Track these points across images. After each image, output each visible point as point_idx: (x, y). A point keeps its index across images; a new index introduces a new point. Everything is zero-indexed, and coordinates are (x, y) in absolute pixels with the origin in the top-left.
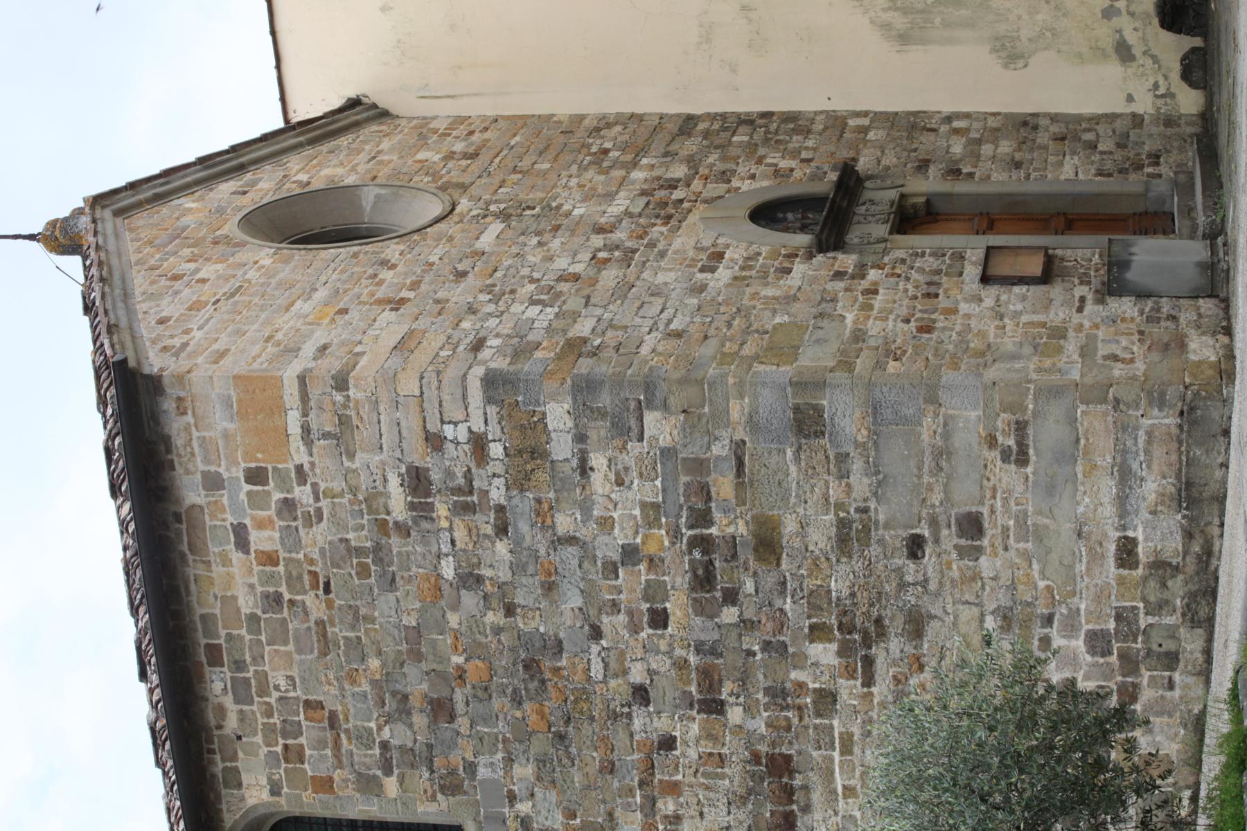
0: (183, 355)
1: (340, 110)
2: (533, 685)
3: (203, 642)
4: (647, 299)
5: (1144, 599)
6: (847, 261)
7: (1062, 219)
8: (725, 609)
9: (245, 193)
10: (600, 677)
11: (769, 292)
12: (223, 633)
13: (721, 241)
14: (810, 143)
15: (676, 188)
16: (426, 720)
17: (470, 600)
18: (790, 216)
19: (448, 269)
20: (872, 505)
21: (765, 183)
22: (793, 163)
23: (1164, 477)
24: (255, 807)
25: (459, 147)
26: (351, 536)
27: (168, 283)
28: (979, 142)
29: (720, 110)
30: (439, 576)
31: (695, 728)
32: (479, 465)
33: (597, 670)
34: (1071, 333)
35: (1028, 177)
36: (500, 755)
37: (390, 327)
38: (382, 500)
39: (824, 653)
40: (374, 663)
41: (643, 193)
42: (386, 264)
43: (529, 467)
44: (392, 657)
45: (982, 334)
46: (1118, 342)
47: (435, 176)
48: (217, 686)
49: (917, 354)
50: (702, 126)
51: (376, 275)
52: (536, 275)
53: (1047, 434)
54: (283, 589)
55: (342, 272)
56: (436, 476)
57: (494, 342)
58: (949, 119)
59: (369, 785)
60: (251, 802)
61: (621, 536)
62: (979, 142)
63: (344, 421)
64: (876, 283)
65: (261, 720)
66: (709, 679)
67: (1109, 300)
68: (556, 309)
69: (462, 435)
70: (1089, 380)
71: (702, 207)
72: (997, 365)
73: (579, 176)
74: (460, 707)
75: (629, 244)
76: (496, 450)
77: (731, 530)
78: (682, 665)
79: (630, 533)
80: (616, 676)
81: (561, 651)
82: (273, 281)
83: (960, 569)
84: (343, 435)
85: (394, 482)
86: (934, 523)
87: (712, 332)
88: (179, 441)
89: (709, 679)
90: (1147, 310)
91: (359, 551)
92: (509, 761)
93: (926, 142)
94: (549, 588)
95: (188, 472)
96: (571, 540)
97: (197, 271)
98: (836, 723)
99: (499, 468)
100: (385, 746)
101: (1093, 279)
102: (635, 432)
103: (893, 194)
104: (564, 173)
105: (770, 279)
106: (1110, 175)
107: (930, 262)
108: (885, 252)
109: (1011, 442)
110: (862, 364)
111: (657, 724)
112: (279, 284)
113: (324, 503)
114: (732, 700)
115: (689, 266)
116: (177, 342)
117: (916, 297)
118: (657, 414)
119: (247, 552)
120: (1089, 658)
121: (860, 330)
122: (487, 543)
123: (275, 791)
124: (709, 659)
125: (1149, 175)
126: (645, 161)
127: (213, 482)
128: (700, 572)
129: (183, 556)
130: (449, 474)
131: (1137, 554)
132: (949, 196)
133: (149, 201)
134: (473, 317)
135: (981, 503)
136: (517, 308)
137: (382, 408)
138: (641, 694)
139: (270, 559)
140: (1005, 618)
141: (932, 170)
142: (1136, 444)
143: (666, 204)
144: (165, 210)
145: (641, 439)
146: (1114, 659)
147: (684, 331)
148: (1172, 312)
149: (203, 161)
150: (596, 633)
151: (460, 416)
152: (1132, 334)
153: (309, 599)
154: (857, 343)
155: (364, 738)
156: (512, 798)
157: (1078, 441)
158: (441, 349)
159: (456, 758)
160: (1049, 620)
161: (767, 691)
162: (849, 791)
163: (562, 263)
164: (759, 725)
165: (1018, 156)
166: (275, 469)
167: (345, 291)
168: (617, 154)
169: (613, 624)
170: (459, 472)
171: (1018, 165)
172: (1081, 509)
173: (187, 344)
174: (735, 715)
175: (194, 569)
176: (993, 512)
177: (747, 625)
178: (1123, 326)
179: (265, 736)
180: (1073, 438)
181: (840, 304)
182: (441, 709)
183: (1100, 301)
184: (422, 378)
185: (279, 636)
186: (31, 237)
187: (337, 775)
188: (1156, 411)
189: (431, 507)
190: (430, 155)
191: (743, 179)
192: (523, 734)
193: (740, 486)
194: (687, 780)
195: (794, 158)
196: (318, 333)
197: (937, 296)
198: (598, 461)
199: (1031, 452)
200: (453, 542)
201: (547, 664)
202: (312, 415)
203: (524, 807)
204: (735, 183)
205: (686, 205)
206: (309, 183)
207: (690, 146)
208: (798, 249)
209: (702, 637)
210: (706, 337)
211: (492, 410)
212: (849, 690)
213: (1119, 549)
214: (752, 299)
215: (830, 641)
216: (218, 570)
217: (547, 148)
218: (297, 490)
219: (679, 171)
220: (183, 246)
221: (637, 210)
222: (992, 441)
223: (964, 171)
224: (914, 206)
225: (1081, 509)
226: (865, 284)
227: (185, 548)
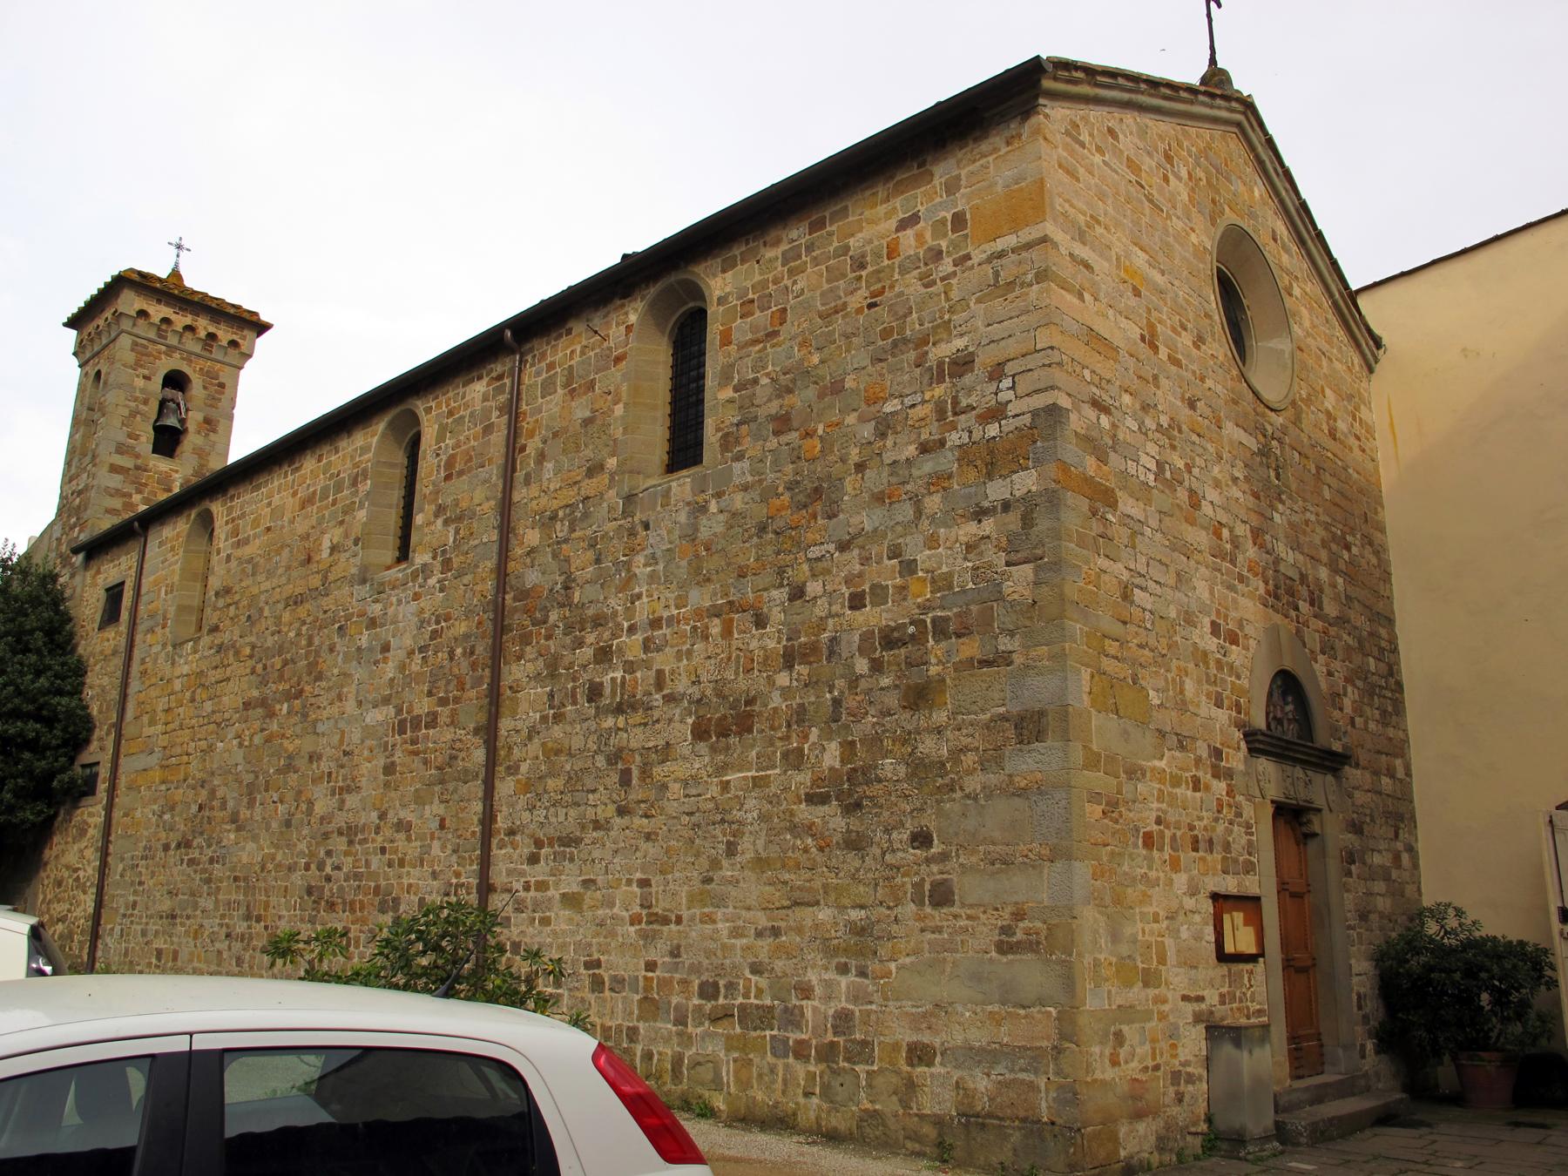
0: (1068, 140)
1: (1369, 331)
2: (801, 497)
3: (827, 214)
4: (1172, 569)
5: (881, 1070)
6: (1236, 759)
7: (1309, 963)
8: (866, 661)
9: (1275, 240)
10: (810, 555)
11: (1189, 686)
12: (834, 228)
13: (1252, 643)
14: (1372, 726)
15: (1312, 604)
16: (773, 412)
17: (867, 431)
18: (1289, 708)
19: (1199, 394)
20: (958, 794)
21: (1324, 686)
22: (1348, 709)
23: (990, 1099)
24: (709, 286)
25: (1342, 426)
26: (914, 315)
27: (1161, 150)
28: (1387, 878)
29: (1401, 648)
30: (885, 400)
31: (771, 644)
32: (978, 416)
33: (815, 552)
34: (1152, 992)
35: (1350, 927)
36: (750, 479)
37: (1123, 332)
38: (945, 336)
39: (832, 756)
40: (816, 359)
41: (1303, 578)
42: (1199, 341)
43: (979, 463)
44: (820, 372)
45: (1145, 899)
46: (1142, 1043)
47: (1308, 401)
48: (794, 234)
49: (1114, 834)
50: (1383, 632)
51: (1185, 329)
52: (1196, 471)
53: (1030, 973)
54: (870, 269)
55: (1187, 301)
56: (968, 379)
57: (1105, 421)
58: (1411, 849)
59: (726, 377)
60: (712, 283)
61: (923, 557)
62: (1387, 878)
63: (1010, 285)
64: (1208, 788)
65: (771, 276)
66: (808, 654)
67: (1201, 1028)
68: (1152, 484)
69: (1005, 396)
70: (1083, 1020)
71: (1292, 627)
72: (1102, 919)
73: (1318, 522)
74: (784, 439)
75: (1240, 558)
76: (993, 430)
77: (933, 660)
78: (821, 626)
79: (927, 565)
80: (811, 569)
81: (830, 518)
82: (1171, 239)
83: (904, 884)
84: (1000, 288)
85: (959, 343)
86: (944, 857)
87: (1132, 628)
88: (985, 146)
89: (808, 654)
90: (1189, 1069)
91: (902, 329)
92: (745, 488)
93: (1382, 830)
94: (879, 498)
95: (959, 162)
96: (919, 513)
97: (1179, 179)
98: (777, 771)
99: (977, 436)
100: (755, 381)
101: (1228, 1006)
102: (1014, 557)
103: (1319, 802)
104: (1321, 510)
105: (1206, 686)
106: (1360, 1008)
107: (1239, 838)
108: (1250, 798)
109: (1019, 936)
110: (1098, 780)
111: (776, 610)
112: (1168, 244)
113: (940, 285)
114: (795, 675)
115: (1218, 612)
116: (1085, 137)
117: (1191, 828)
118: (1031, 577)
119: (897, 230)
120: (831, 1012)
121: (1144, 775)
122: (914, 436)
123: (722, 301)
124: (825, 652)
125: (1363, 1046)
126: (1340, 580)
127: (952, 187)
128: (896, 634)
129: (892, 178)
130: (970, 391)
131: (919, 1065)
132: (1323, 853)
133: (1257, 157)
134: (1138, 406)
135: (963, 905)
136: (1152, 449)
137: (1023, 318)
138: (798, 593)
139: (892, 252)
140: (863, 929)
141: (1350, 839)
142: (1022, 1070)
143: (1293, 595)
144: (1249, 170)
145: (1008, 564)
146: (830, 1037)
147: (1132, 602)
148: (1187, 1098)
149: (1304, 206)
150: (843, 547)
151: (1020, 390)
152: (1154, 1058)
153: (863, 292)
154: (1126, 772)
155: (759, 365)
156: (719, 495)
157: (1024, 1007)
158: (1093, 372)
159: (747, 443)
160: (862, 973)
161: (802, 706)
162: (725, 786)
163: (1212, 495)
164: (776, 700)
165: (1373, 917)
166: (966, 236)
167: (1164, 300)
168: (1346, 556)
169: (851, 561)
170: (973, 400)
171: (1363, 917)
172: (960, 1009)
173: (1083, 145)
174: (783, 679)
175: (881, 191)
176: (955, 917)
177: (854, 682)
178: (1164, 1045)
179: (759, 282)
180: (1026, 1003)
181: (1177, 754)
182: (782, 423)
183: (1198, 1018)
184: (1052, 348)
185: (834, 275)
186: (1213, 61)
187: (733, 348)
188: (1053, 1094)
189: (941, 380)
190: (1330, 400)
191: (1327, 665)
192: (768, 494)
193: (970, 663)
194: (734, 643)
195: (1355, 710)
196: (1106, 264)
197: (1196, 850)
198: (988, 526)
199: (1010, 957)
200: (913, 406)
201: (818, 507)
202: (1014, 257)
203: (713, 507)
204: (1321, 658)
205: (1293, 614)
206: (1291, 295)
207: (1360, 620)
208: (1247, 714)
209: (843, 643)
210: (1125, 623)
211: (1027, 419)
212: (802, 779)
213: (925, 1046)
214: (1178, 668)
215: (842, 761)
216: (882, 209)
217: (1346, 498)
218: (950, 260)
219: (1331, 609)
220: (1207, 172)
221: (1282, 568)
222: (1019, 916)
223: (1353, 867)
224: (1310, 821)
225: (960, 1009)
226: (1206, 776)
227: (898, 178)
